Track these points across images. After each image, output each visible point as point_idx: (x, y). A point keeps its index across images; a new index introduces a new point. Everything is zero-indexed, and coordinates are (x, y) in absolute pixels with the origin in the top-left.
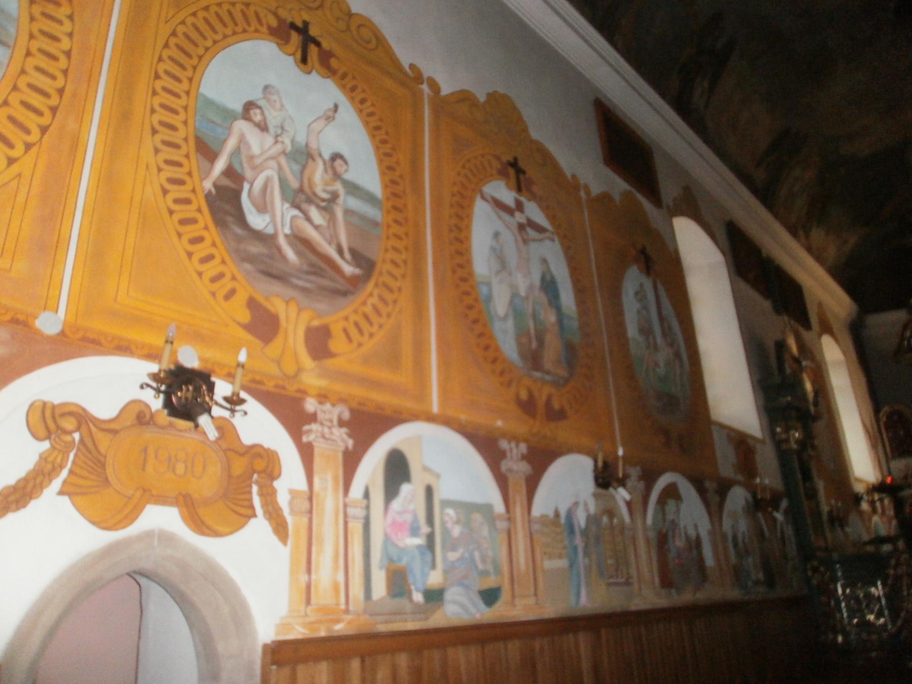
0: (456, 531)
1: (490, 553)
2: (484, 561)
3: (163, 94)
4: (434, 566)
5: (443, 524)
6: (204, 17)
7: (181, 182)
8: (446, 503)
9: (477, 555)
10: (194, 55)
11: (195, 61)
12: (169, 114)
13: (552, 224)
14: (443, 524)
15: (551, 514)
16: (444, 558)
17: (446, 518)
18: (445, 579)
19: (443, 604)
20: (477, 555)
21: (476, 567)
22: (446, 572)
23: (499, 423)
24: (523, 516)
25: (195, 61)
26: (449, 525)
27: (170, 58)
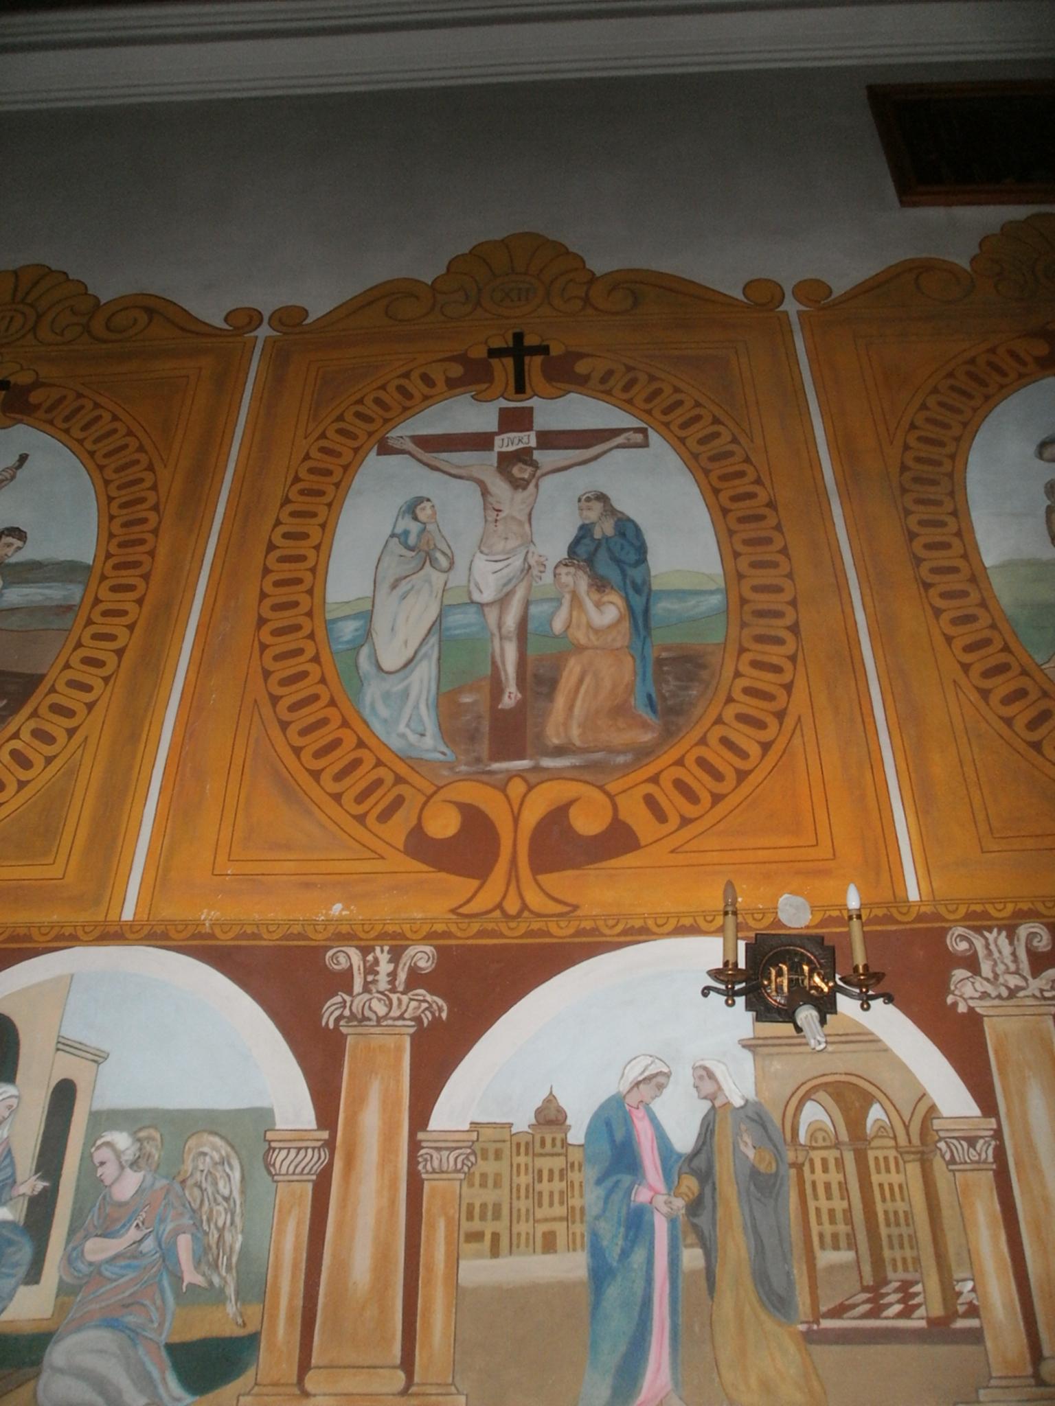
0: (127, 1186)
1: (236, 1241)
2: (205, 1257)
3: (735, 506)
4: (34, 1275)
5: (88, 1166)
6: (939, 483)
7: (969, 619)
8: (103, 1120)
9: (184, 1245)
10: (702, 448)
11: (952, 526)
12: (753, 525)
13: (628, 405)
14: (88, 1166)
15: (523, 1121)
16: (70, 1260)
17: (103, 1154)
18: (61, 1309)
19: (37, 1375)
20: (184, 1245)
21: (177, 1278)
22: (64, 1290)
23: (337, 909)
24: (388, 1138)
25: (952, 526)
26: (108, 1173)
27: (921, 523)
